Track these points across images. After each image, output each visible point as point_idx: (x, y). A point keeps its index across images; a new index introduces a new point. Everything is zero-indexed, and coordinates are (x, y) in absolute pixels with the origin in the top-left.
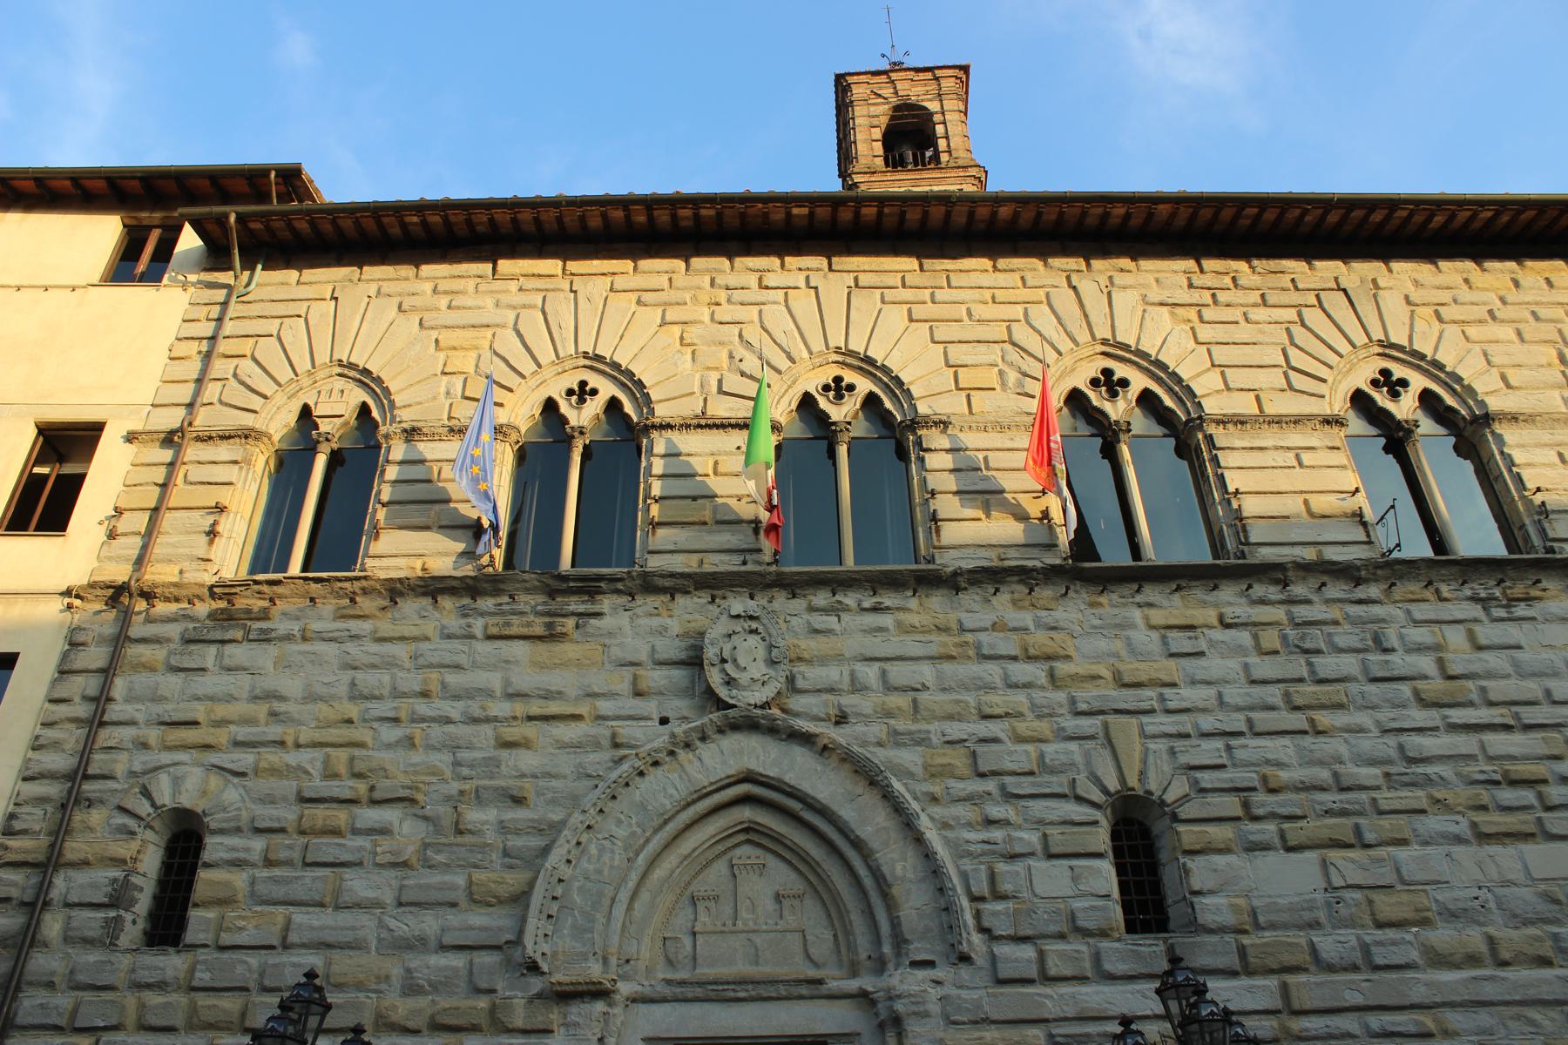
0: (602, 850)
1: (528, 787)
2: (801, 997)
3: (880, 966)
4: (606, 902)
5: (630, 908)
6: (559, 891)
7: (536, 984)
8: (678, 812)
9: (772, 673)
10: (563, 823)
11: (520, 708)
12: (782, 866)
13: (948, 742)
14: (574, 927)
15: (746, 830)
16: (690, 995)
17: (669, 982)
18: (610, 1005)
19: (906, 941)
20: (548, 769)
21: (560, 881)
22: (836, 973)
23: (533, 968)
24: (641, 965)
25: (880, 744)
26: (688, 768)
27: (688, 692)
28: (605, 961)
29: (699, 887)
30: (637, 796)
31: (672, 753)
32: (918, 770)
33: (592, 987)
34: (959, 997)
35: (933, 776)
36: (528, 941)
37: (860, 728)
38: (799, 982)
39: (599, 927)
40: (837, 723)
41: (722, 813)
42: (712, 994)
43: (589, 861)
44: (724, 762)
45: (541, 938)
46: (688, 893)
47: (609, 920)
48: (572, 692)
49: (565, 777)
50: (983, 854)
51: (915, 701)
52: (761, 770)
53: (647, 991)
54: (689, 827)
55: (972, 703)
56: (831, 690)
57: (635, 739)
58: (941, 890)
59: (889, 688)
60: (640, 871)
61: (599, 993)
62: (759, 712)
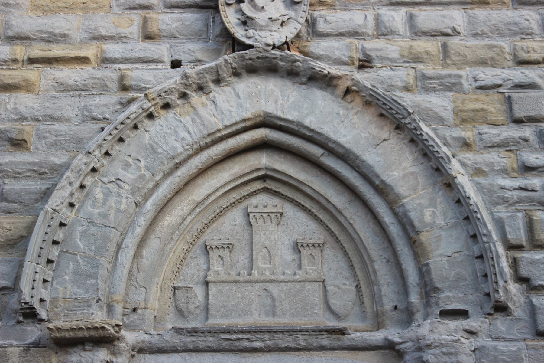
0: (108, 194)
1: (28, 130)
2: (322, 348)
3: (407, 316)
4: (112, 247)
5: (137, 256)
6: (60, 235)
7: (33, 332)
8: (190, 157)
9: (292, 14)
10: (66, 166)
11: (20, 51)
12: (301, 216)
13: (481, 88)
14: (76, 272)
15: (263, 178)
16: (201, 345)
17: (178, 331)
18: (114, 354)
19: (436, 290)
20: (50, 112)
21: (62, 225)
22: (360, 325)
23: (30, 314)
24: (149, 315)
25: (407, 89)
26: (202, 111)
27: (200, 35)
28: (110, 308)
29: (211, 236)
30: (146, 139)
31: (184, 96)
32: (449, 116)
33: (93, 333)
34: (495, 348)
35: (464, 121)
36: (25, 286)
37: (385, 73)
38: (319, 331)
39: (103, 272)
40: (361, 67)
41: (237, 159)
42: (225, 344)
43: (94, 205)
44: (240, 106)
45: (39, 284)
46: (201, 242)
47: (114, 266)
48: (77, 35)
49: (68, 120)
50: (520, 201)
51: (445, 46)
52: (279, 114)
53: (155, 340)
54: (202, 172)
55: (507, 49)
56: (354, 34)
57: (144, 81)
58: (474, 237)
59: (417, 33)
60: (149, 216)
61: (102, 340)
62: (277, 52)
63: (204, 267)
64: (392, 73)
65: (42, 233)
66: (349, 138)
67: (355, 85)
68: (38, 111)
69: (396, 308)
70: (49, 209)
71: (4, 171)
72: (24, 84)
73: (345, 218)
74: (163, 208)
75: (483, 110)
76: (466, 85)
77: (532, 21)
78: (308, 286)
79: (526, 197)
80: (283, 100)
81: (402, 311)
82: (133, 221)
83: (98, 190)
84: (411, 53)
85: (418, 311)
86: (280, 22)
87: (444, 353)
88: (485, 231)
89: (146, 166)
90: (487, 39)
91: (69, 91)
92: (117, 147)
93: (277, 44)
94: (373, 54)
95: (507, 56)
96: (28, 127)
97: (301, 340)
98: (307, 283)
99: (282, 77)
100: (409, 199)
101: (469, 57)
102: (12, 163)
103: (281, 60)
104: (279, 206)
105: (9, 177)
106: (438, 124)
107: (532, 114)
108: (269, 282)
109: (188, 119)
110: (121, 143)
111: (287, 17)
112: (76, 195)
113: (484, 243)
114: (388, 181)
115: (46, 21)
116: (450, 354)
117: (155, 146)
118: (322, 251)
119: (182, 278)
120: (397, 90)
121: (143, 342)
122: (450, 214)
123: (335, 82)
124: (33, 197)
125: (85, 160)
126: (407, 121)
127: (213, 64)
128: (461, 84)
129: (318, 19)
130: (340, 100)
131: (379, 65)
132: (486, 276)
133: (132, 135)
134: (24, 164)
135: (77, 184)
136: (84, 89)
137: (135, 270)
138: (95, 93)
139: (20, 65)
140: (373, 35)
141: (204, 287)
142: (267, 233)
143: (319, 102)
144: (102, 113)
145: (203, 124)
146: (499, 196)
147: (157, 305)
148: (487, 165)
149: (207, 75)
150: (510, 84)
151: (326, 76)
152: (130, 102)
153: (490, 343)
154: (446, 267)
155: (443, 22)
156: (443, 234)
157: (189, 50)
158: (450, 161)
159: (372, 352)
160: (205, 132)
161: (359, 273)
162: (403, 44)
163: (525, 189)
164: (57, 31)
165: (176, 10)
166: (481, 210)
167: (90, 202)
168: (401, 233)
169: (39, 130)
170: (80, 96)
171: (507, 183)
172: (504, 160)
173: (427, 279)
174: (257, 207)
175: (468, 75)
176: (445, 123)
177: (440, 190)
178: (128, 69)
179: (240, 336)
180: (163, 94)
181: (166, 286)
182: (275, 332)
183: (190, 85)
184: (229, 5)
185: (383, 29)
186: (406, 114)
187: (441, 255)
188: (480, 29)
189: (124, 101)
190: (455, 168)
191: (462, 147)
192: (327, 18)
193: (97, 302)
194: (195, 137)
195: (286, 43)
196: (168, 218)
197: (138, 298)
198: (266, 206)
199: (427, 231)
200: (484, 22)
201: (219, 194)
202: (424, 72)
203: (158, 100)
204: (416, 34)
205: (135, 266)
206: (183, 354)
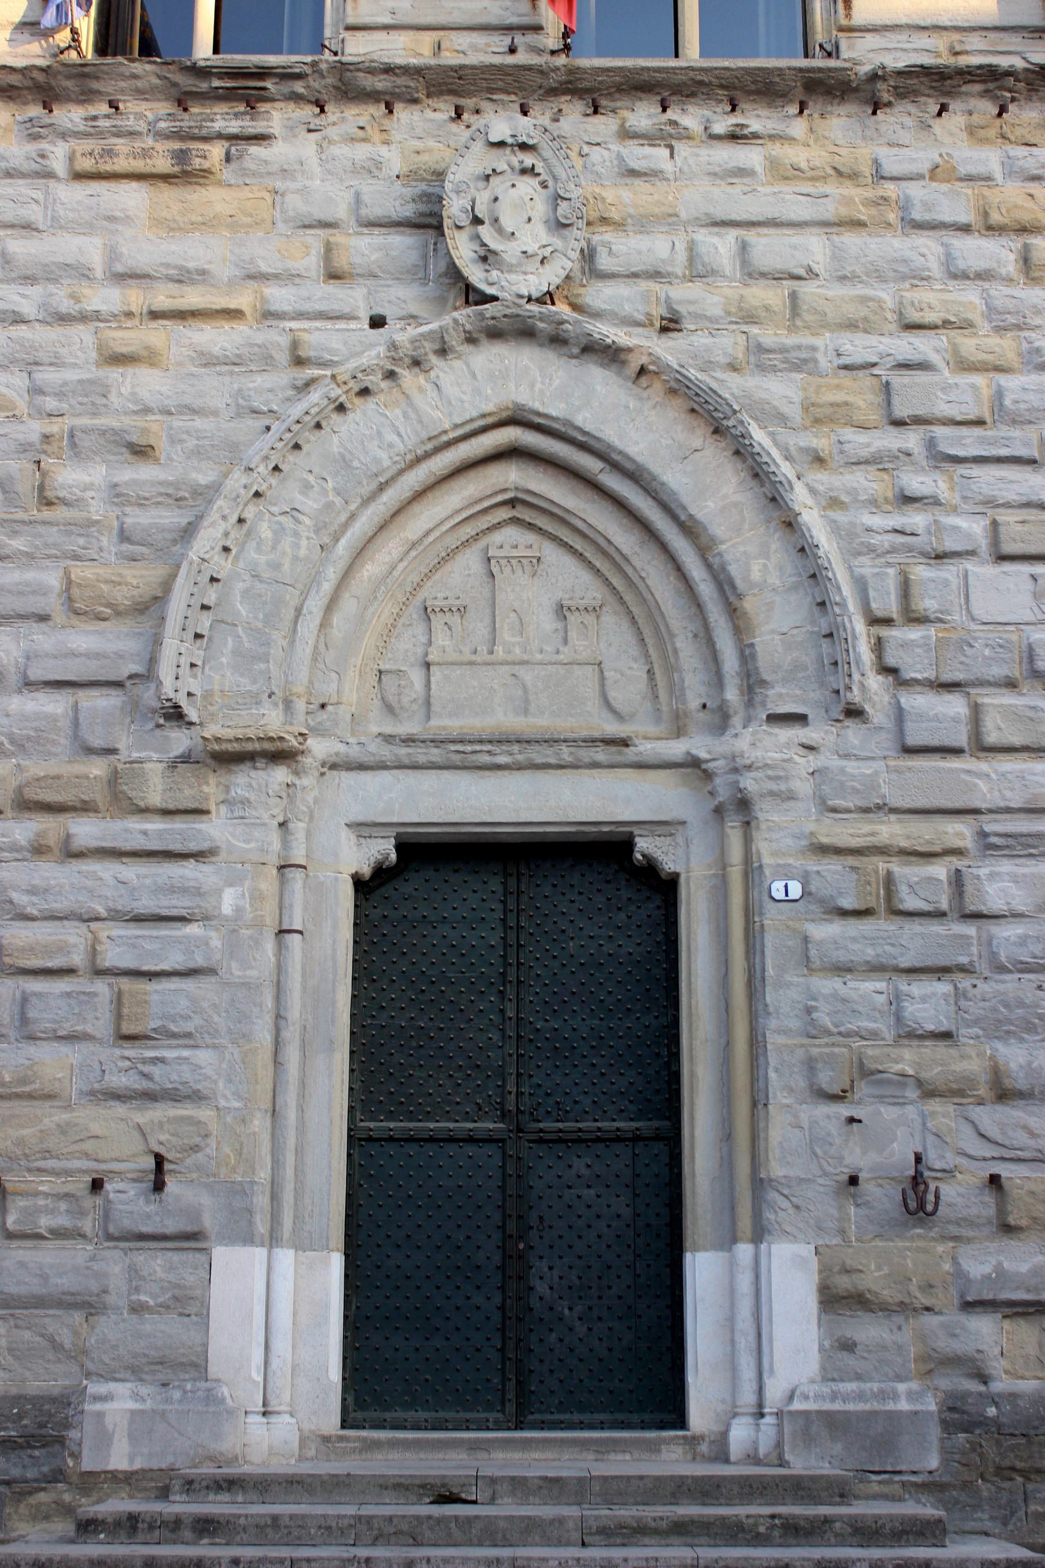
0: (279, 532)
2: (595, 765)
3: (721, 720)
4: (289, 614)
6: (211, 597)
7: (180, 740)
8: (401, 472)
9: (558, 243)
10: (215, 488)
11: (136, 298)
12: (568, 561)
13: (846, 367)
14: (237, 652)
15: (512, 503)
16: (422, 759)
17: (388, 739)
18: (296, 773)
19: (763, 683)
20: (187, 400)
21: (213, 580)
22: (652, 729)
23: (175, 715)
24: (344, 712)
25: (733, 367)
26: (418, 400)
27: (418, 274)
28: (288, 705)
29: (434, 592)
31: (391, 375)
32: (794, 412)
33: (267, 746)
34: (842, 770)
35: (817, 421)
36: (165, 672)
37: (701, 340)
39: (276, 652)
40: (664, 330)
41: (472, 474)
42: (457, 759)
43: (258, 550)
44: (477, 392)
45: (185, 670)
47: (292, 642)
48: (224, 272)
49: (215, 413)
50: (893, 550)
51: (793, 296)
52: (537, 406)
53: (354, 752)
55: (890, 303)
56: (655, 275)
57: (330, 351)
58: (822, 604)
59: (752, 274)
60: (342, 565)
61: (280, 755)
62: (534, 308)
63: (424, 639)
64: (712, 340)
65: (186, 594)
66: (642, 446)
67: (653, 363)
68: (169, 397)
69: (704, 706)
70: (195, 558)
71: (124, 495)
72: (145, 353)
73: (635, 569)
75: (846, 404)
76: (823, 362)
77: (930, 257)
78: (578, 671)
79: (902, 544)
80: (542, 383)
81: (713, 711)
82: (318, 573)
83: (265, 525)
84: (741, 309)
85: (736, 713)
86: (540, 257)
87: (769, 778)
88: (838, 599)
89: (334, 489)
90: (860, 286)
91: (214, 365)
92: (291, 458)
93: (535, 294)
94: (682, 309)
95: (889, 316)
96: (154, 423)
97: (566, 753)
98: (576, 667)
99: (541, 345)
100: (729, 544)
101: (830, 315)
102: (135, 482)
103: (541, 320)
104: (535, 546)
105: (131, 504)
106: (778, 425)
107: (920, 412)
108: (519, 664)
109: (398, 412)
110: (297, 452)
111: (550, 249)
112: (232, 536)
113: (836, 615)
115: (173, 247)
116: (778, 778)
117: (348, 457)
118: (598, 617)
119: (390, 655)
120: (718, 370)
121: (337, 754)
122: (789, 569)
123: (622, 356)
124: (169, 536)
125: (244, 480)
126: (730, 423)
127: (434, 326)
128: (816, 361)
129: (599, 249)
130: (630, 384)
131: (692, 327)
132: (836, 663)
133: (313, 438)
134: (153, 484)
135: (234, 518)
137: (321, 646)
138: (254, 369)
139: (136, 322)
140: (684, 276)
141: (424, 671)
142: (517, 589)
143: (599, 388)
144: (267, 402)
145: (421, 422)
146: (862, 543)
147: (354, 697)
148: (848, 493)
149: (426, 344)
150: (890, 362)
151: (609, 347)
153: (835, 763)
154: (780, 649)
155: (793, 256)
156: (778, 599)
157: (399, 298)
158: (792, 488)
159: (668, 771)
160: (425, 435)
161: (652, 651)
162: (729, 292)
164: (191, 265)
165: (376, 231)
166: (834, 566)
167: (254, 544)
168: (716, 595)
169: (171, 428)
170: (232, 373)
171: (877, 521)
172: (874, 485)
173: (750, 667)
174: (501, 547)
175: (826, 346)
176: (789, 424)
177: (775, 531)
178: (304, 330)
179: (478, 747)
180: (359, 375)
181: (368, 669)
182: (528, 742)
183: (401, 359)
184: (459, 228)
185: (700, 267)
186: (729, 413)
187: (773, 632)
188: (850, 269)
189: (299, 383)
190: (801, 498)
191: (812, 462)
192: (613, 247)
193: (270, 697)
194: (409, 443)
195: (549, 293)
196: (368, 567)
197: (328, 689)
198: (516, 547)
199: (755, 595)
200: (857, 258)
201: (444, 528)
202: (761, 340)
203: (351, 383)
204: (750, 275)
205: (322, 639)
206: (394, 772)
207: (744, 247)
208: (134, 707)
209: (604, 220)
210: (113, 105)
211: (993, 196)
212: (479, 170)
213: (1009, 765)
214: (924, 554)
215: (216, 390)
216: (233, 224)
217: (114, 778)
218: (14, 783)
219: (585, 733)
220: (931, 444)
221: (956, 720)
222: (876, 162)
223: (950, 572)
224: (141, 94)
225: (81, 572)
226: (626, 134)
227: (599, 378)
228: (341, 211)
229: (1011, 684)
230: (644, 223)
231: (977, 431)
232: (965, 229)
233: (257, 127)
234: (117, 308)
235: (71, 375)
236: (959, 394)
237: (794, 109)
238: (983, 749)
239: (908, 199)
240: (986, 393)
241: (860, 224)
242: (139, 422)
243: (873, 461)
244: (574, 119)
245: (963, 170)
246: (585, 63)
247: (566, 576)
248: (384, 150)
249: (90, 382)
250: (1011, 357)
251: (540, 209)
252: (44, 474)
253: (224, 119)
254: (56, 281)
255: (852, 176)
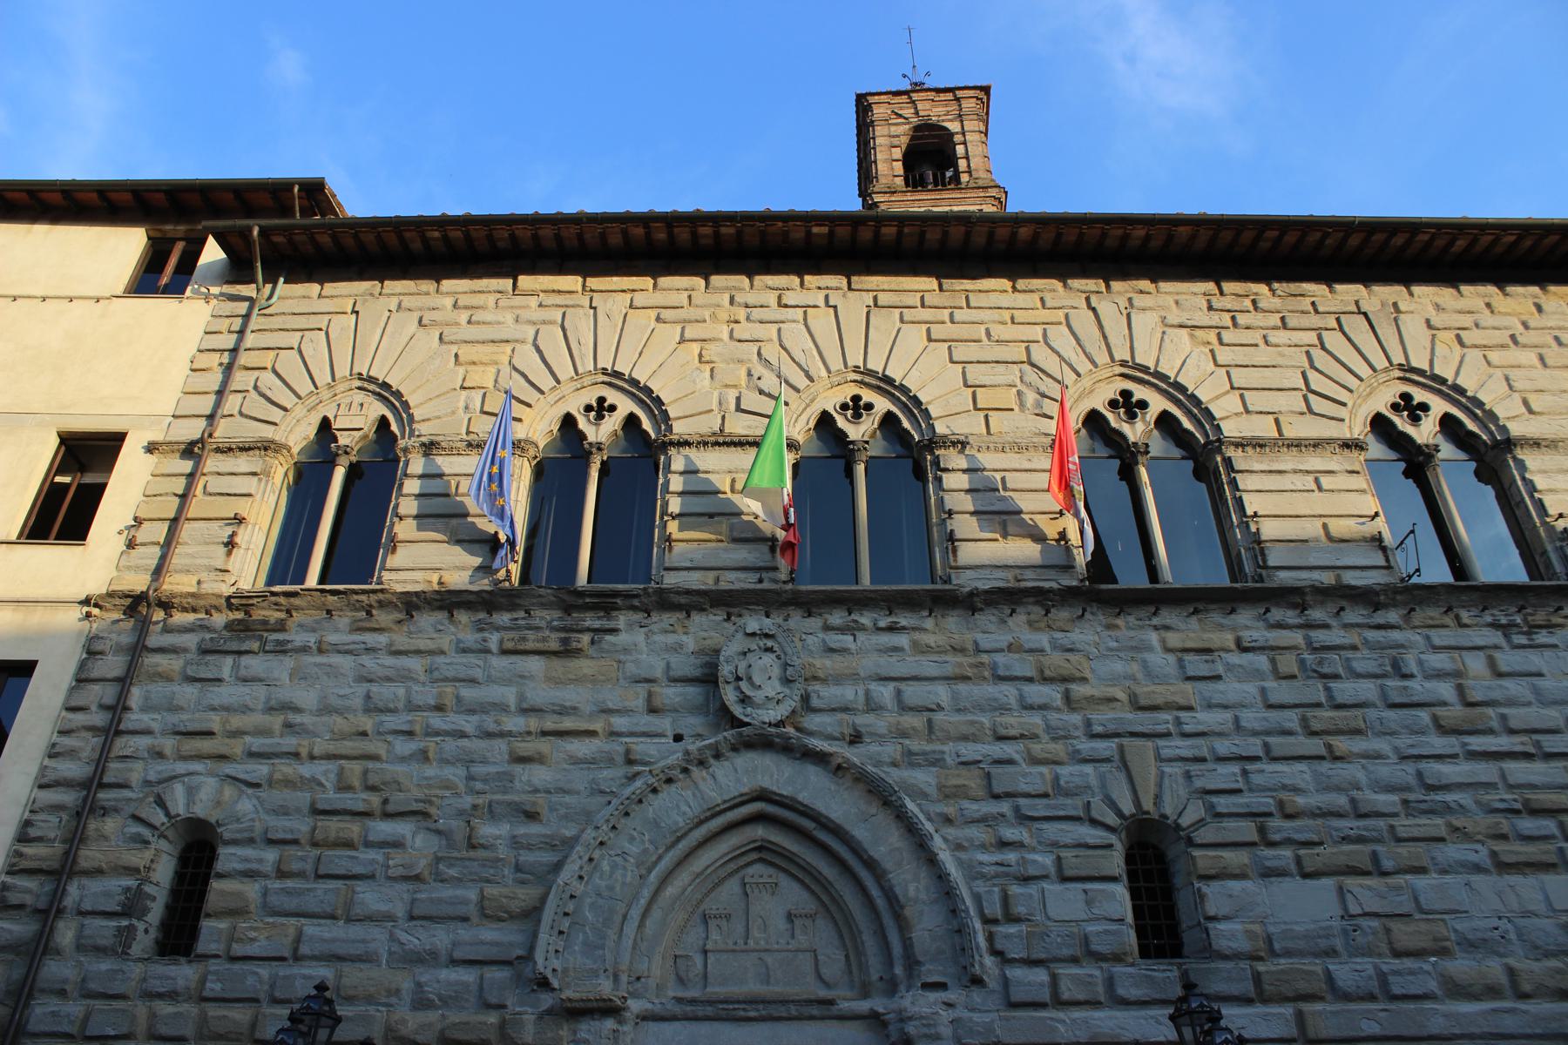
0: (614, 866)
2: (812, 1018)
3: (892, 988)
6: (570, 907)
7: (546, 1000)
8: (691, 830)
9: (787, 691)
10: (575, 839)
11: (533, 723)
12: (795, 886)
15: (759, 849)
16: (700, 1014)
17: (679, 1000)
18: (620, 1023)
19: (918, 963)
21: (572, 897)
22: (849, 994)
23: (544, 984)
24: (652, 983)
25: (894, 764)
26: (702, 785)
28: (616, 977)
29: (711, 906)
30: (650, 813)
31: (685, 770)
32: (932, 791)
33: (601, 1004)
34: (971, 1020)
35: (947, 796)
36: (539, 957)
38: (809, 1002)
40: (852, 743)
41: (734, 831)
43: (601, 878)
44: (738, 780)
45: (552, 954)
47: (620, 936)
49: (578, 793)
50: (997, 876)
51: (930, 721)
52: (774, 789)
53: (658, 1009)
56: (845, 709)
58: (954, 911)
59: (904, 708)
60: (653, 888)
61: (609, 1010)
62: (772, 730)
74: (664, 881)
76: (949, 760)
78: (801, 956)
94: (863, 730)
96: (540, 799)
97: (793, 1010)
102: (526, 835)
114: (876, 856)
116: (929, 1026)
136: (593, 761)
147: (658, 973)
150: (989, 759)
152: (633, 777)
153: (966, 1014)
157: (691, 723)
163: (1002, 865)
197: (642, 967)
207: (899, 693)
208: (518, 979)
209: (815, 678)
210: (527, 612)
211: (1046, 661)
212: (740, 649)
213: (1077, 1014)
214: (1017, 878)
215: (580, 779)
216: (593, 680)
217: (503, 1025)
218: (439, 1027)
219: (805, 997)
220: (1017, 809)
221: (1042, 985)
222: (976, 643)
223: (1033, 889)
224: (543, 606)
225: (491, 890)
226: (827, 628)
227: (813, 774)
228: (658, 673)
229: (1074, 960)
230: (839, 679)
231: (1045, 801)
232: (1030, 680)
233: (612, 624)
234: (523, 729)
235: (492, 769)
236: (1033, 778)
237: (926, 613)
238: (1059, 1003)
239: (995, 663)
240: (1048, 777)
241: (969, 678)
242: (531, 798)
243: (982, 820)
244: (797, 620)
245: (1027, 646)
246: (803, 588)
247: (793, 895)
248: (684, 638)
249: (504, 773)
250: (1063, 755)
251: (776, 671)
252: (472, 829)
253: (591, 620)
254: (487, 713)
255: (962, 651)
